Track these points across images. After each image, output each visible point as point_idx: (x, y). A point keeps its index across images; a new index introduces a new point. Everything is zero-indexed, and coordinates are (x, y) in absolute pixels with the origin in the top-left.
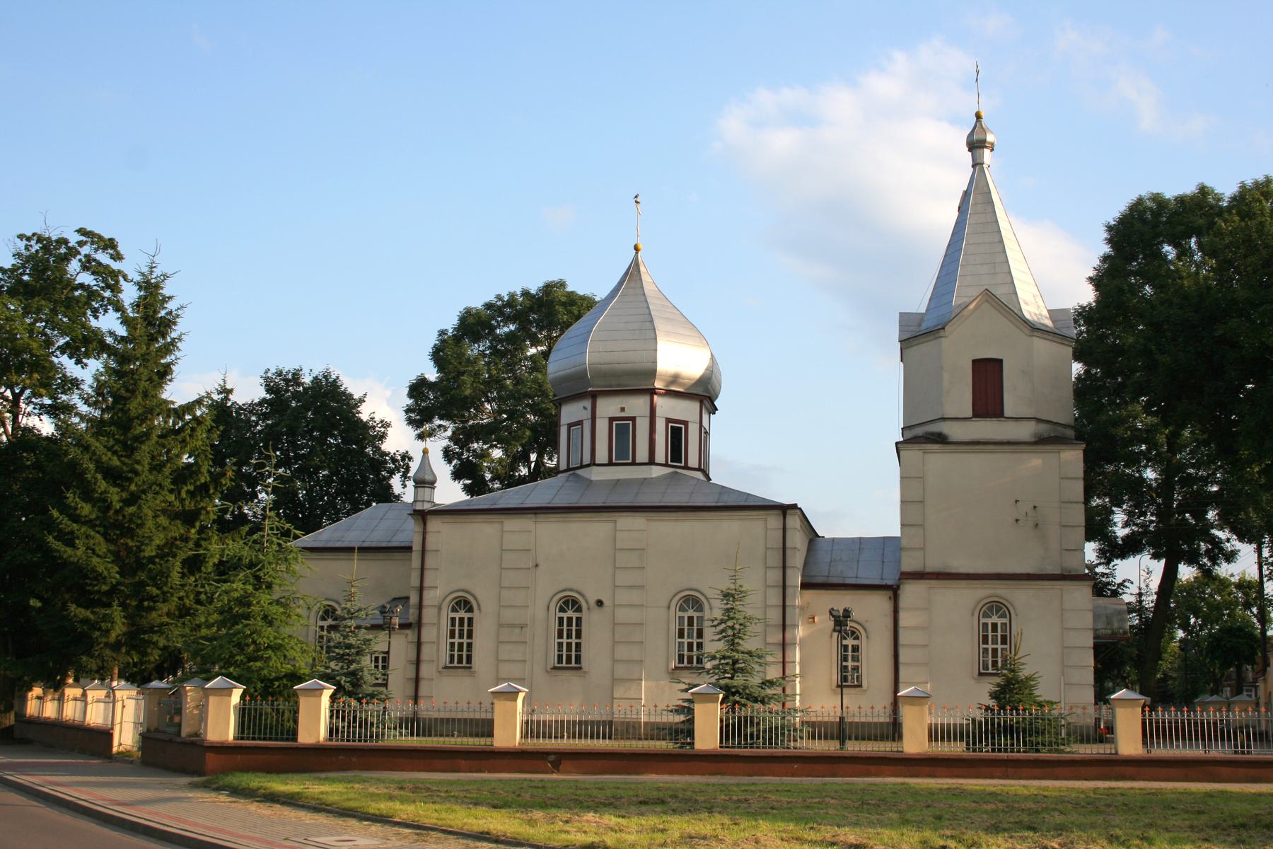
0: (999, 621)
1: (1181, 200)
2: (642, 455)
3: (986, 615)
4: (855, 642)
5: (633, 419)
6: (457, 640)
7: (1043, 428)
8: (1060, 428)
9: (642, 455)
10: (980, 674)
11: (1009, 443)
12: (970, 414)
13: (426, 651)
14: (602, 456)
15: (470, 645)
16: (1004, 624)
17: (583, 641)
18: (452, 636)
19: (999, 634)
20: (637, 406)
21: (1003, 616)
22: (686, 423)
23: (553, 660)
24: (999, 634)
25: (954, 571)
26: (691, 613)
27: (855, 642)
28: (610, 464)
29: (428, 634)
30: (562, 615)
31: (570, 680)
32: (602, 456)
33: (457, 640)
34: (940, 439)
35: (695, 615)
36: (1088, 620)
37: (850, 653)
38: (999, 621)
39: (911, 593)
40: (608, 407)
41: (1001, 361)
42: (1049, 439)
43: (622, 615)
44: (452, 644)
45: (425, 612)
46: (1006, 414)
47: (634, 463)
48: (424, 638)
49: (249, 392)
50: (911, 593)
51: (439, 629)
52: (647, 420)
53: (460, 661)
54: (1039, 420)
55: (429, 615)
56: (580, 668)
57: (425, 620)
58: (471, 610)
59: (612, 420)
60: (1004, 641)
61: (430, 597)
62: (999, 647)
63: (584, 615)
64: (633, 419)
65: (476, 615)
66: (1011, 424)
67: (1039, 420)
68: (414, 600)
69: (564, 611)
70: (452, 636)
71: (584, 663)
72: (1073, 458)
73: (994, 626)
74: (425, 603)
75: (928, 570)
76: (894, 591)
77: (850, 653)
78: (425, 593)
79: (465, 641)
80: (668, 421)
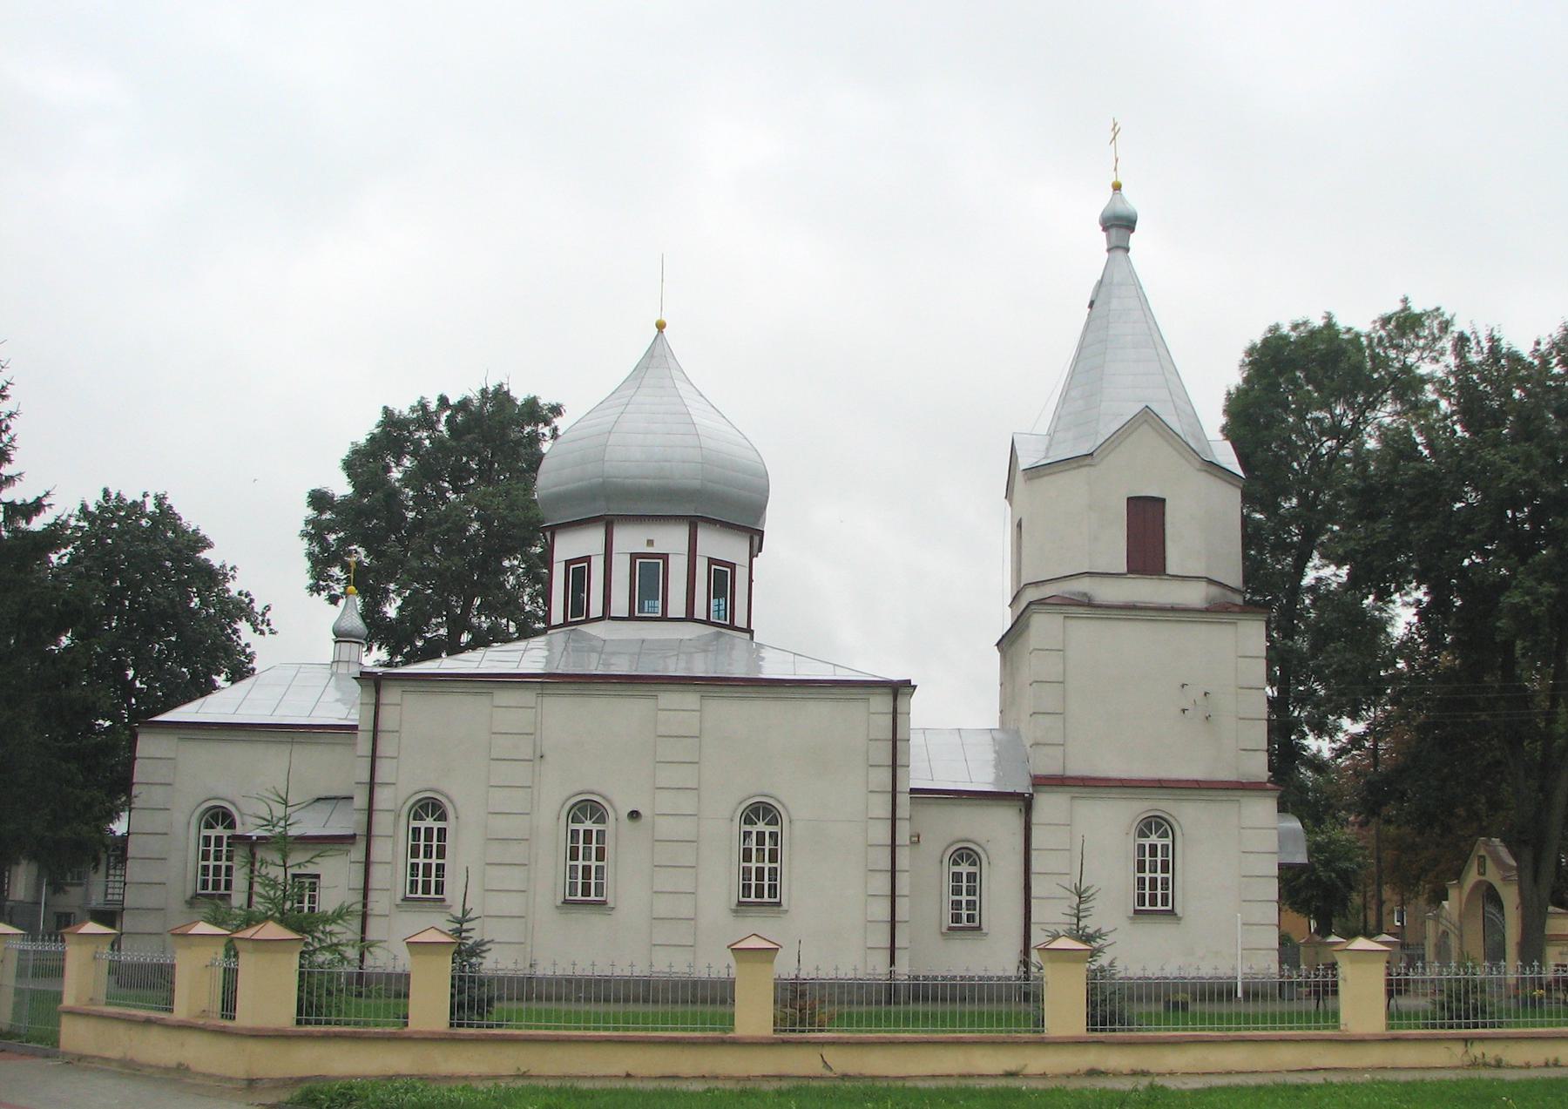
0: (1159, 842)
1: (373, 439)
2: (596, 609)
3: (209, 826)
4: (972, 869)
5: (665, 557)
6: (421, 860)
7: (1214, 591)
8: (1229, 593)
9: (677, 607)
10: (1136, 912)
11: (1173, 609)
12: (1124, 569)
13: (377, 874)
14: (620, 605)
15: (440, 868)
16: (1165, 847)
17: (607, 864)
18: (415, 854)
19: (1159, 859)
20: (672, 540)
21: (1165, 835)
22: (732, 566)
23: (735, 894)
24: (1159, 859)
25: (1102, 775)
26: (588, 825)
27: (972, 869)
28: (631, 617)
29: (381, 850)
30: (416, 824)
31: (593, 922)
32: (620, 605)
33: (421, 860)
34: (1087, 604)
35: (595, 828)
36: (1272, 842)
37: (964, 884)
38: (1159, 842)
39: (1048, 806)
40: (629, 540)
41: (1132, 501)
42: (1216, 610)
43: (666, 827)
44: (415, 867)
45: (377, 817)
46: (1169, 571)
47: (664, 618)
48: (376, 855)
49: (19, 502)
50: (1048, 806)
51: (395, 844)
52: (685, 559)
53: (426, 890)
54: (1210, 581)
55: (382, 823)
56: (443, 900)
57: (377, 829)
58: (442, 817)
59: (634, 557)
60: (1165, 869)
61: (383, 797)
62: (1159, 875)
63: (609, 827)
64: (665, 557)
65: (450, 825)
66: (1176, 585)
67: (1210, 581)
68: (361, 801)
69: (752, 823)
70: (415, 854)
71: (609, 895)
72: (1252, 636)
73: (1153, 848)
74: (378, 805)
75: (1069, 773)
76: (1025, 803)
77: (964, 884)
78: (378, 791)
79: (434, 861)
80: (711, 561)
